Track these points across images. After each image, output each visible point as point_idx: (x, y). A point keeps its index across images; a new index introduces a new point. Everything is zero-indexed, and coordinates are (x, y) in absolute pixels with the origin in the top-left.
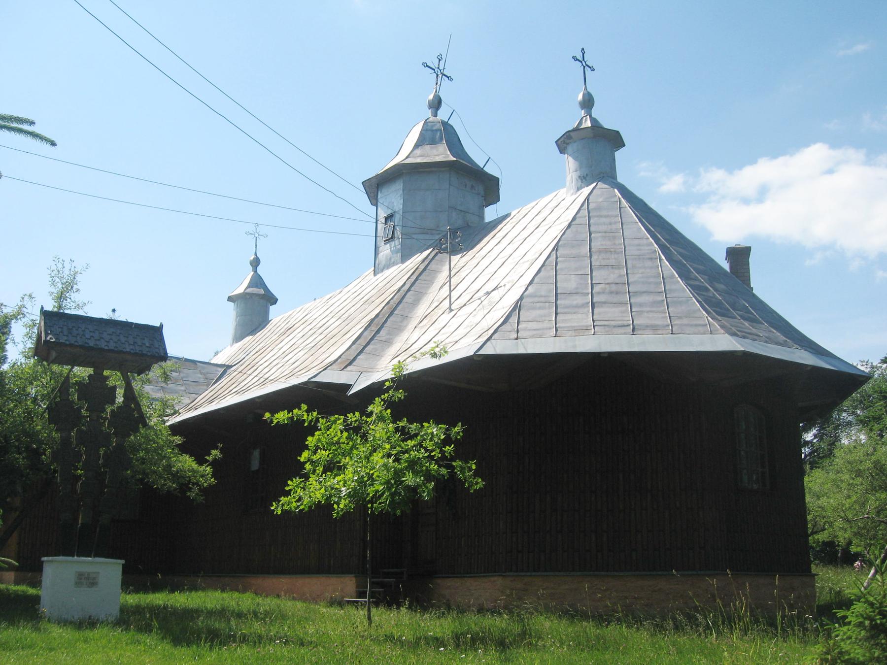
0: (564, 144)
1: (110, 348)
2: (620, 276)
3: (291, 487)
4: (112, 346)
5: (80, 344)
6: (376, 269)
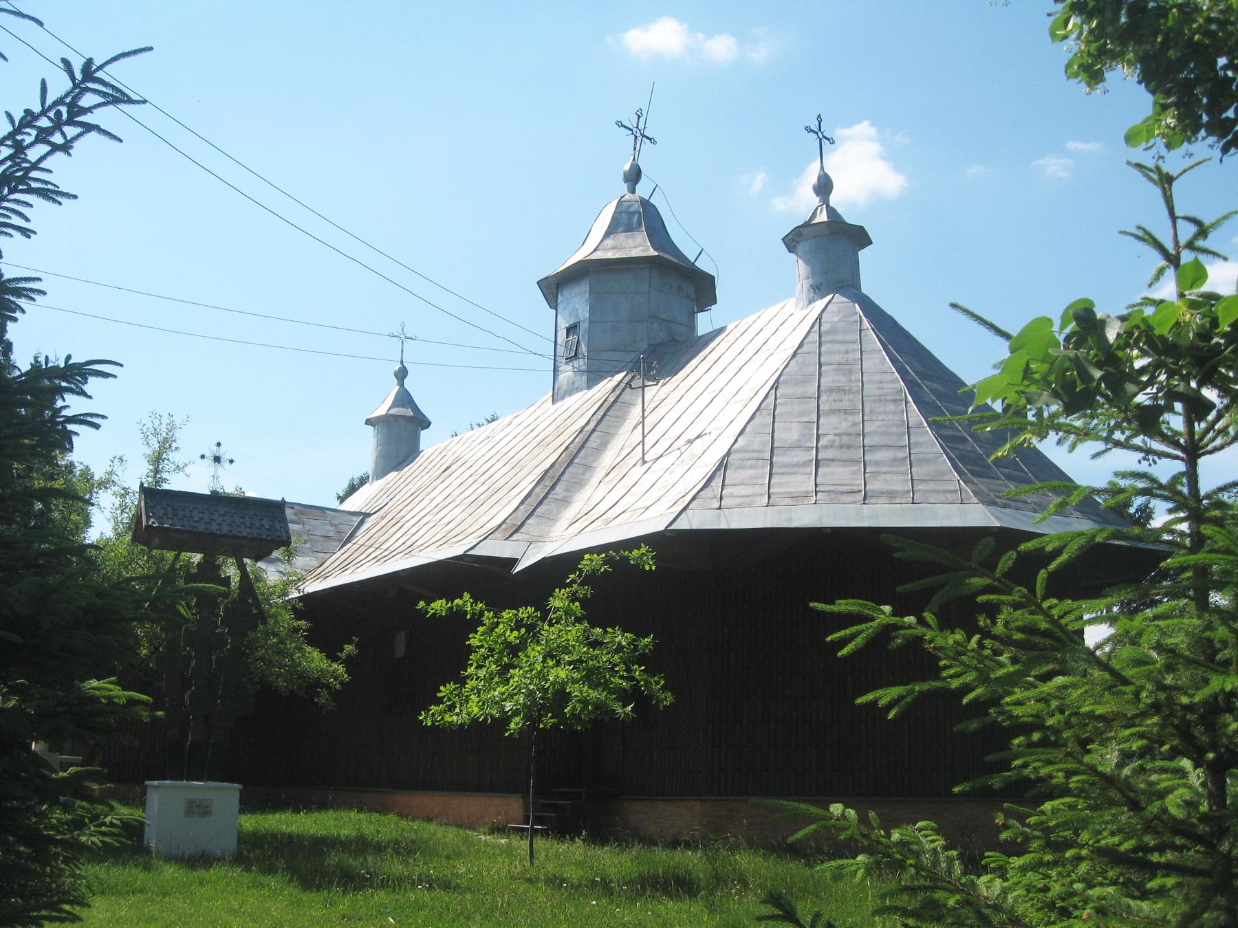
0: (793, 241)
1: (223, 532)
2: (855, 424)
3: (443, 694)
4: (225, 529)
5: (187, 528)
6: (555, 395)
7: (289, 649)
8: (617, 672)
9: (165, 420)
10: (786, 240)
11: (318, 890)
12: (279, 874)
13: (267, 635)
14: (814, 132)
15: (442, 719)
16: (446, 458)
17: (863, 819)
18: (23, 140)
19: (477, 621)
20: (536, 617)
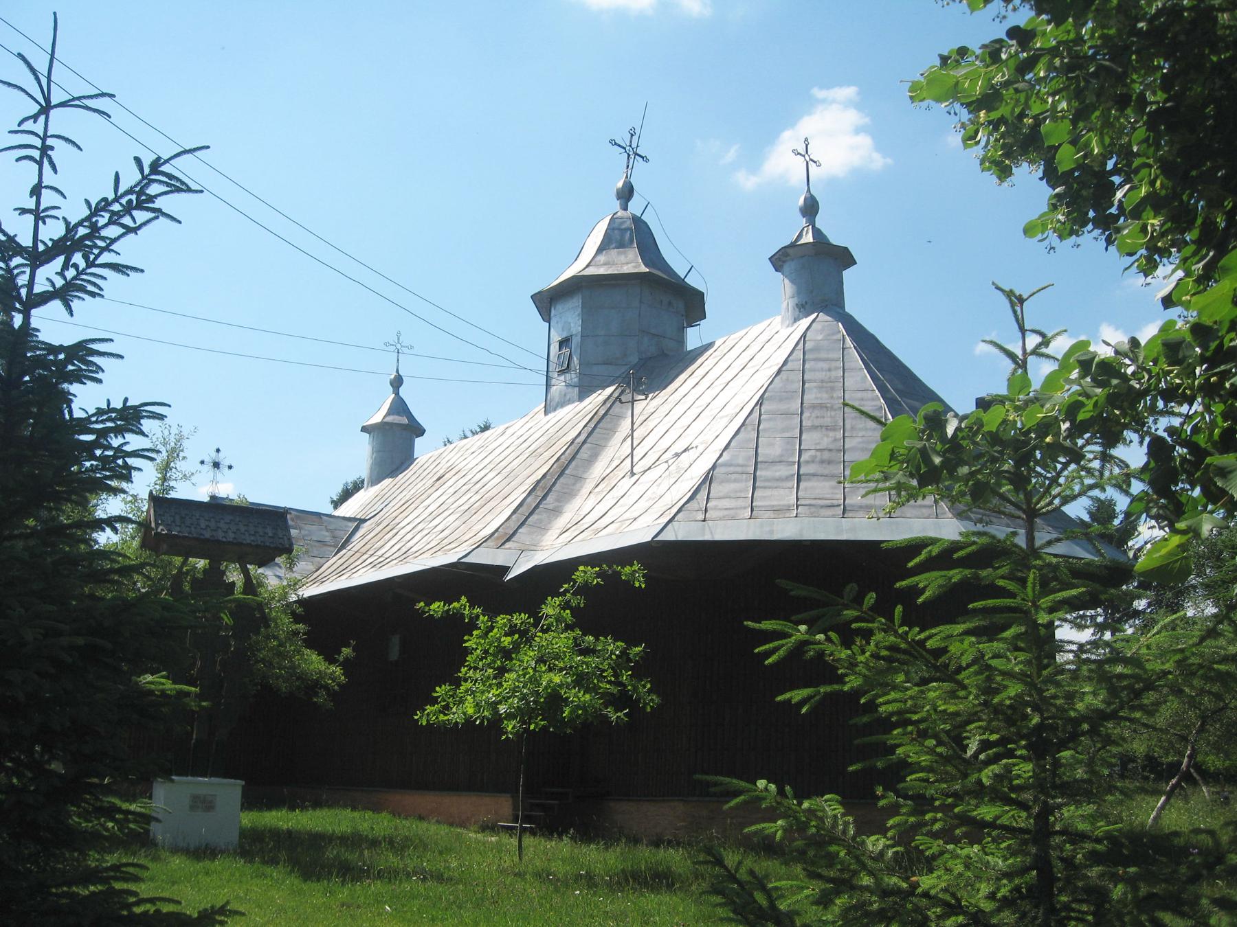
0: (779, 260)
2: (835, 440)
3: (438, 694)
4: (231, 536)
6: (548, 407)
7: (288, 652)
8: (605, 677)
9: (174, 431)
10: (773, 259)
11: (318, 881)
12: (280, 867)
13: (268, 638)
14: (801, 155)
15: (437, 718)
16: (440, 466)
17: (781, 792)
18: (97, 221)
19: (472, 625)
20: (529, 623)
